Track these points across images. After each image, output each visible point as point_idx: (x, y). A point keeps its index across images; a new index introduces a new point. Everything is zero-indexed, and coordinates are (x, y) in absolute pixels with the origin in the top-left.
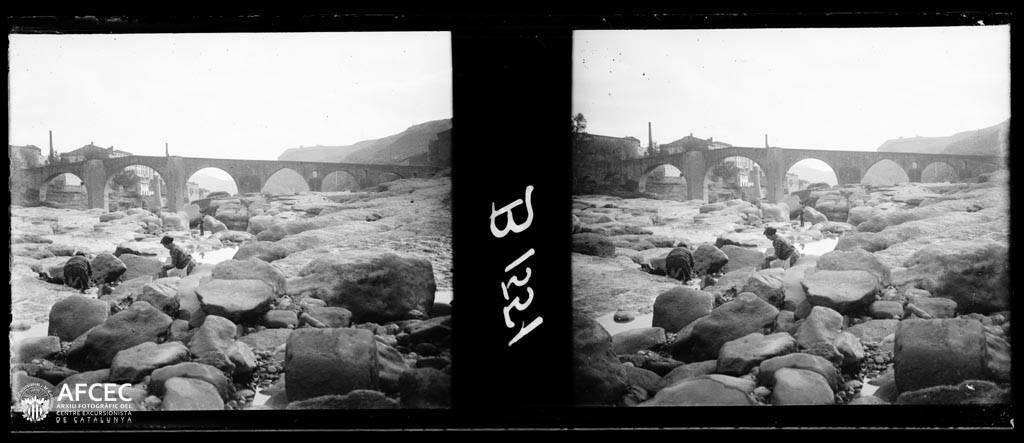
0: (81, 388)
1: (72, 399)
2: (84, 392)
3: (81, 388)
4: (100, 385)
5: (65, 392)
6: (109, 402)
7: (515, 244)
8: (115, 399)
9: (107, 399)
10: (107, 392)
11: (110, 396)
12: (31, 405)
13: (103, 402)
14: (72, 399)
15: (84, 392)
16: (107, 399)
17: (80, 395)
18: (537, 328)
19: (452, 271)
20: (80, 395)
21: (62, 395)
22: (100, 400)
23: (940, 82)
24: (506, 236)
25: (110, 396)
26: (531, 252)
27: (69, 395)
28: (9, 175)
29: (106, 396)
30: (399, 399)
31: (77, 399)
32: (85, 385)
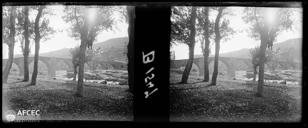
0: (33, 112)
1: (22, 115)
2: (25, 113)
3: (24, 112)
4: (30, 111)
5: (20, 113)
6: (33, 116)
7: (149, 65)
8: (34, 115)
9: (32, 115)
10: (32, 113)
11: (33, 114)
12: (9, 116)
13: (31, 116)
14: (22, 115)
15: (25, 113)
16: (32, 115)
17: (24, 113)
18: (152, 71)
19: (128, 65)
20: (24, 113)
21: (19, 113)
22: (30, 115)
23: (285, 25)
24: (153, 61)
25: (33, 114)
26: (152, 69)
27: (21, 113)
28: (36, 19)
29: (32, 114)
30: (170, 92)
31: (23, 115)
32: (34, 111)
